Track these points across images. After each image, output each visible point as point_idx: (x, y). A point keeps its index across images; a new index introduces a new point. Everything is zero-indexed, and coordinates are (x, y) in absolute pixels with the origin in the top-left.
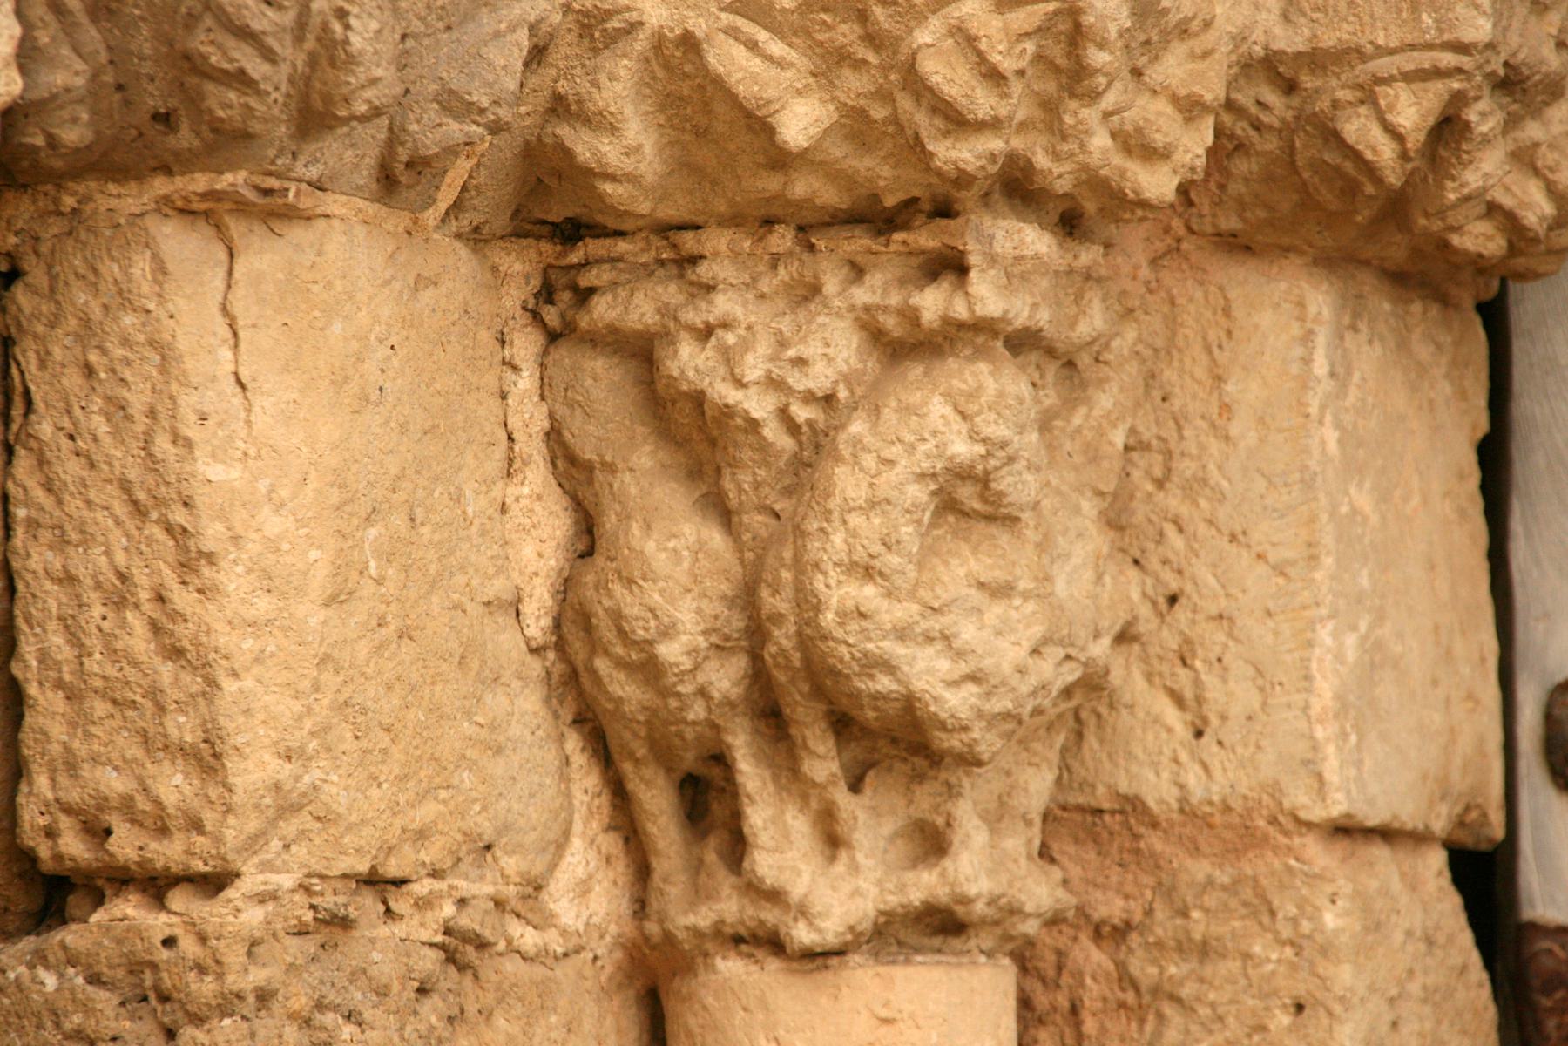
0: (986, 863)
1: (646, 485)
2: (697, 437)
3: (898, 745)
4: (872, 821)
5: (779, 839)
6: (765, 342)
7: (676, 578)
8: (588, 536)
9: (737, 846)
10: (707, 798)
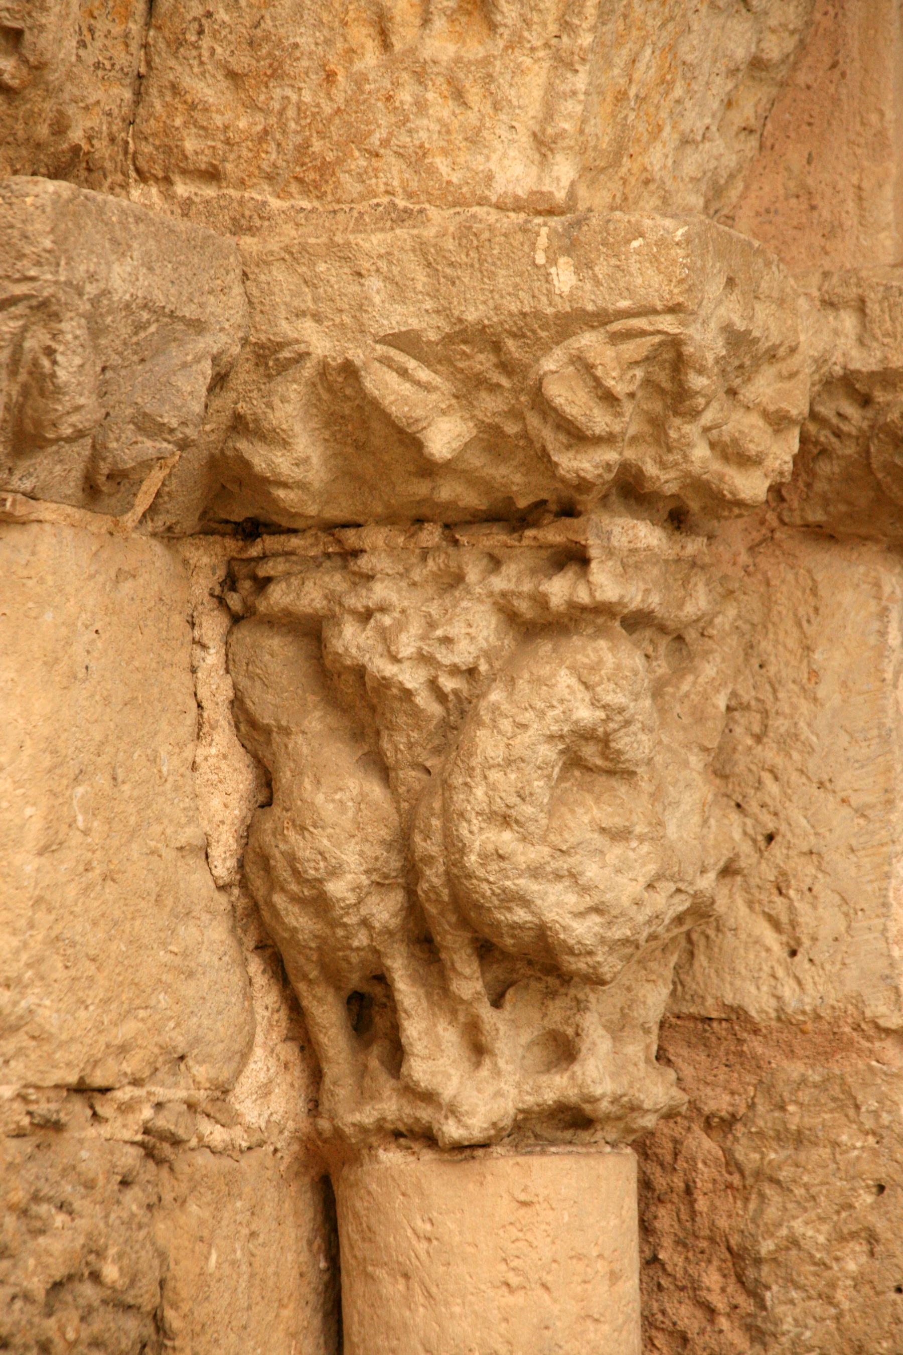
0: (607, 1069)
1: (316, 746)
2: (360, 705)
3: (531, 966)
4: (513, 1032)
5: (432, 1048)
6: (418, 623)
7: (342, 825)
8: (267, 789)
9: (396, 1055)
10: (370, 1013)
